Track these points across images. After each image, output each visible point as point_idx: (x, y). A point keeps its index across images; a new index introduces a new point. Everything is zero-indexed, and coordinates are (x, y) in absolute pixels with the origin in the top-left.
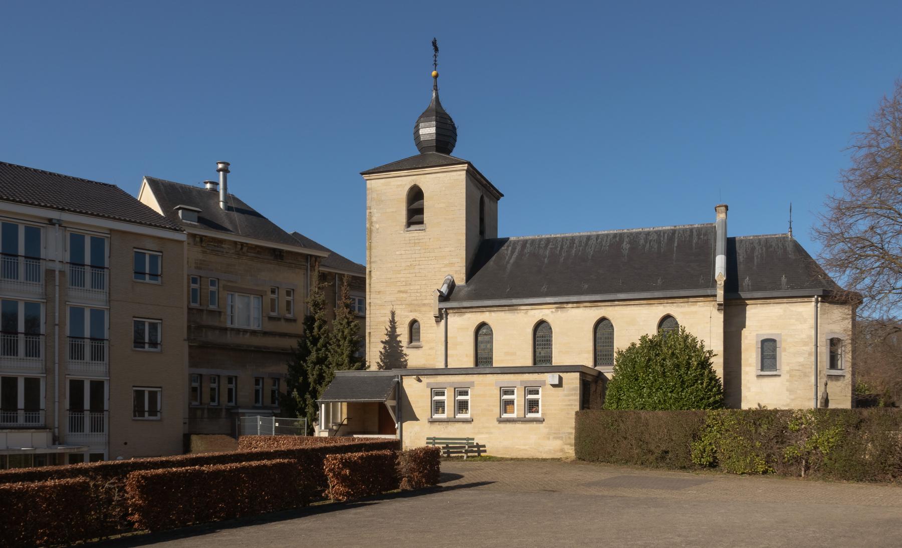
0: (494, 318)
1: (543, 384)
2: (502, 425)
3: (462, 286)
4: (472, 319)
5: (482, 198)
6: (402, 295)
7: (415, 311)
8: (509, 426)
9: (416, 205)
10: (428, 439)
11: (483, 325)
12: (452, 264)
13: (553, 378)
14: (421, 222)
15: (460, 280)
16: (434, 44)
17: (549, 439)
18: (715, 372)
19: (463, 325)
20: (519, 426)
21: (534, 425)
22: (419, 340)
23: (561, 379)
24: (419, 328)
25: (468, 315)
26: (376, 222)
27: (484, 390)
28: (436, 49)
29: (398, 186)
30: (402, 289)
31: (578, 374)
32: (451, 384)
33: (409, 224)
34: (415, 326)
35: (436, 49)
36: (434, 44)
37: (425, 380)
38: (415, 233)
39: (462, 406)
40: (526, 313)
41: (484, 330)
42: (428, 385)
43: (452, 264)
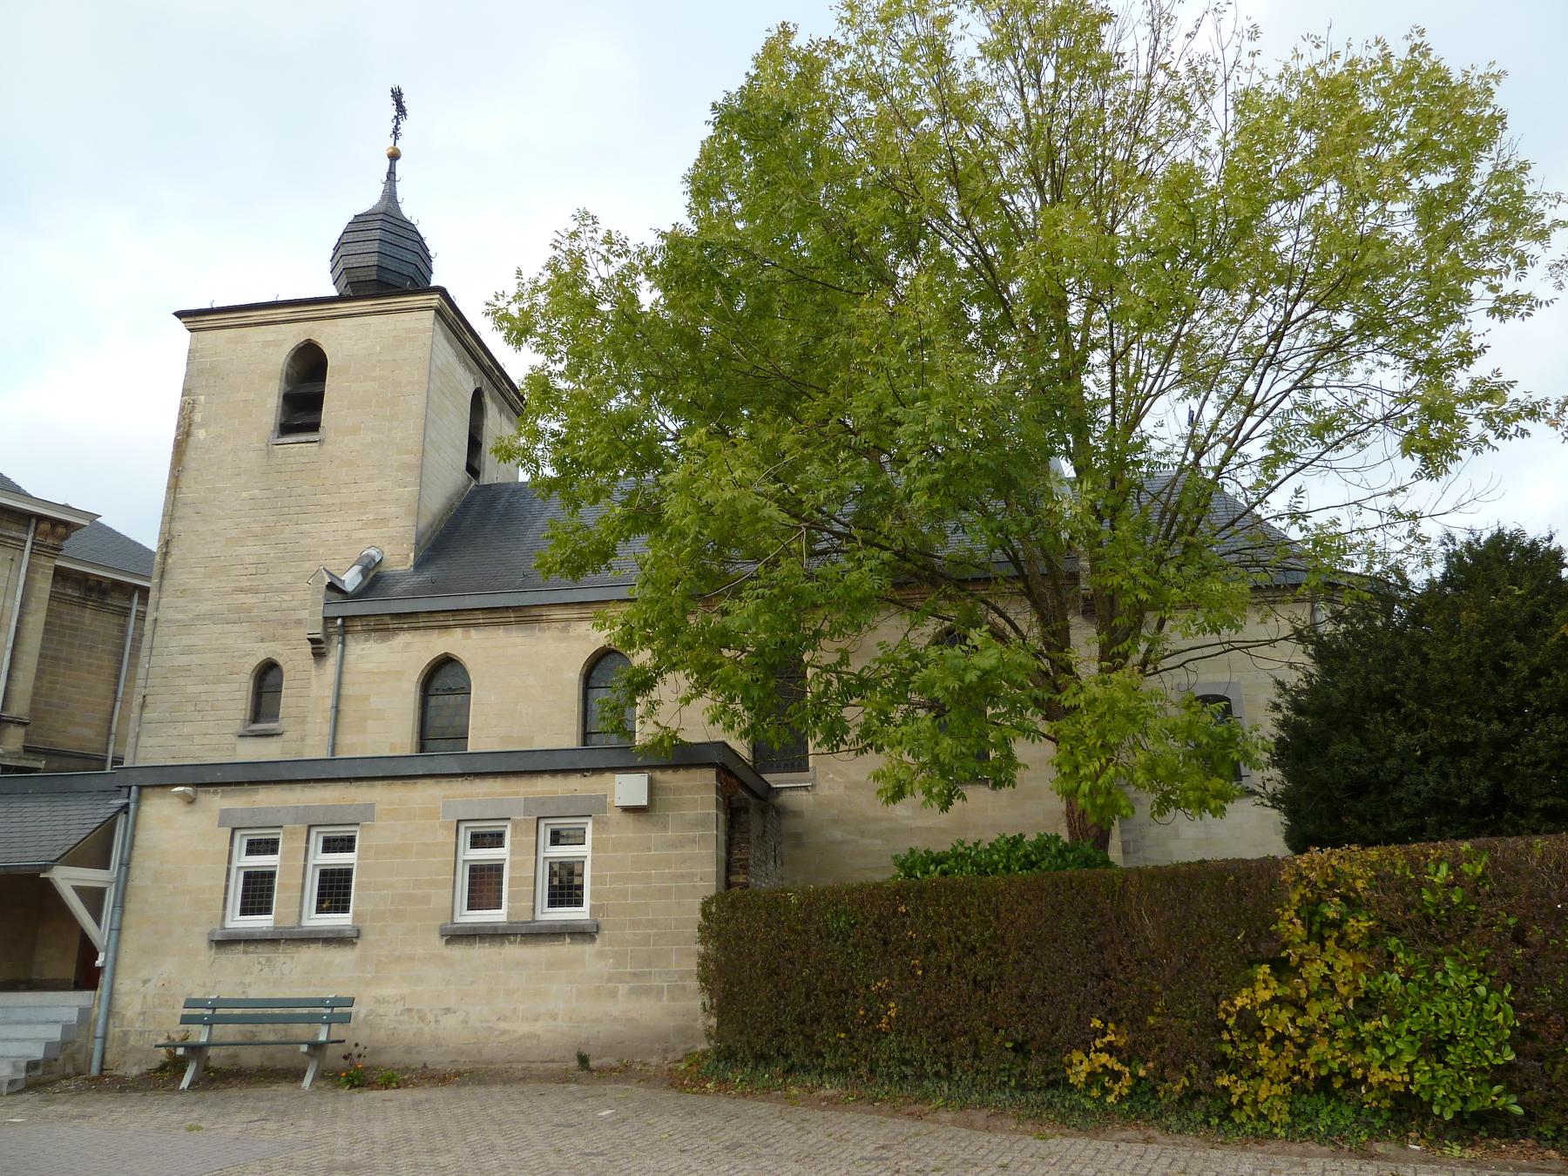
0: (470, 646)
1: (595, 808)
2: (459, 952)
3: (403, 575)
4: (413, 651)
5: (477, 397)
6: (242, 598)
7: (274, 639)
8: (480, 953)
9: (310, 388)
10: (190, 1003)
11: (445, 663)
12: (382, 521)
13: (630, 788)
14: (314, 427)
15: (399, 556)
16: (397, 96)
17: (613, 994)
18: (912, 851)
19: (388, 667)
20: (513, 951)
21: (566, 949)
22: (274, 716)
23: (652, 788)
24: (280, 685)
25: (403, 639)
26: (200, 426)
27: (411, 838)
28: (401, 109)
29: (267, 344)
30: (245, 584)
31: (709, 776)
32: (299, 814)
33: (286, 429)
34: (271, 678)
35: (401, 109)
36: (397, 96)
37: (216, 802)
38: (298, 448)
39: (334, 891)
40: (565, 630)
41: (445, 680)
42: (224, 817)
43: (382, 521)
